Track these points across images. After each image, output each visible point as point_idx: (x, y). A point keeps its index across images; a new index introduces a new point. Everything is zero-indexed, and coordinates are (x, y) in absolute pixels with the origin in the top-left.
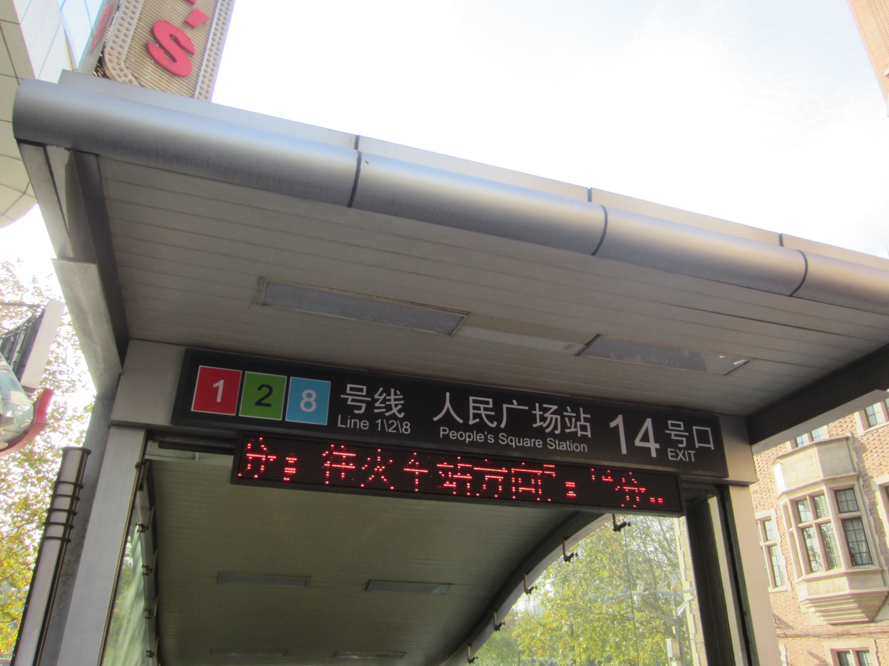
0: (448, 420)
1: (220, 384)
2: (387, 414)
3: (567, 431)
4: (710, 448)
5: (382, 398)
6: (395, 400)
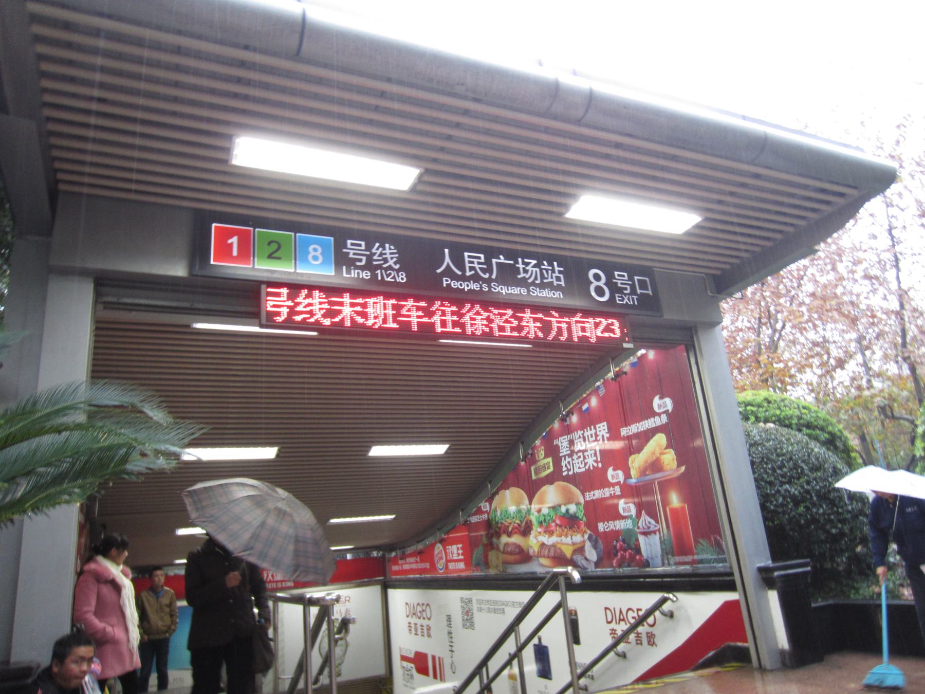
0: (448, 272)
1: (234, 240)
2: (385, 266)
3: (545, 281)
4: (648, 294)
5: (379, 252)
6: (391, 254)
